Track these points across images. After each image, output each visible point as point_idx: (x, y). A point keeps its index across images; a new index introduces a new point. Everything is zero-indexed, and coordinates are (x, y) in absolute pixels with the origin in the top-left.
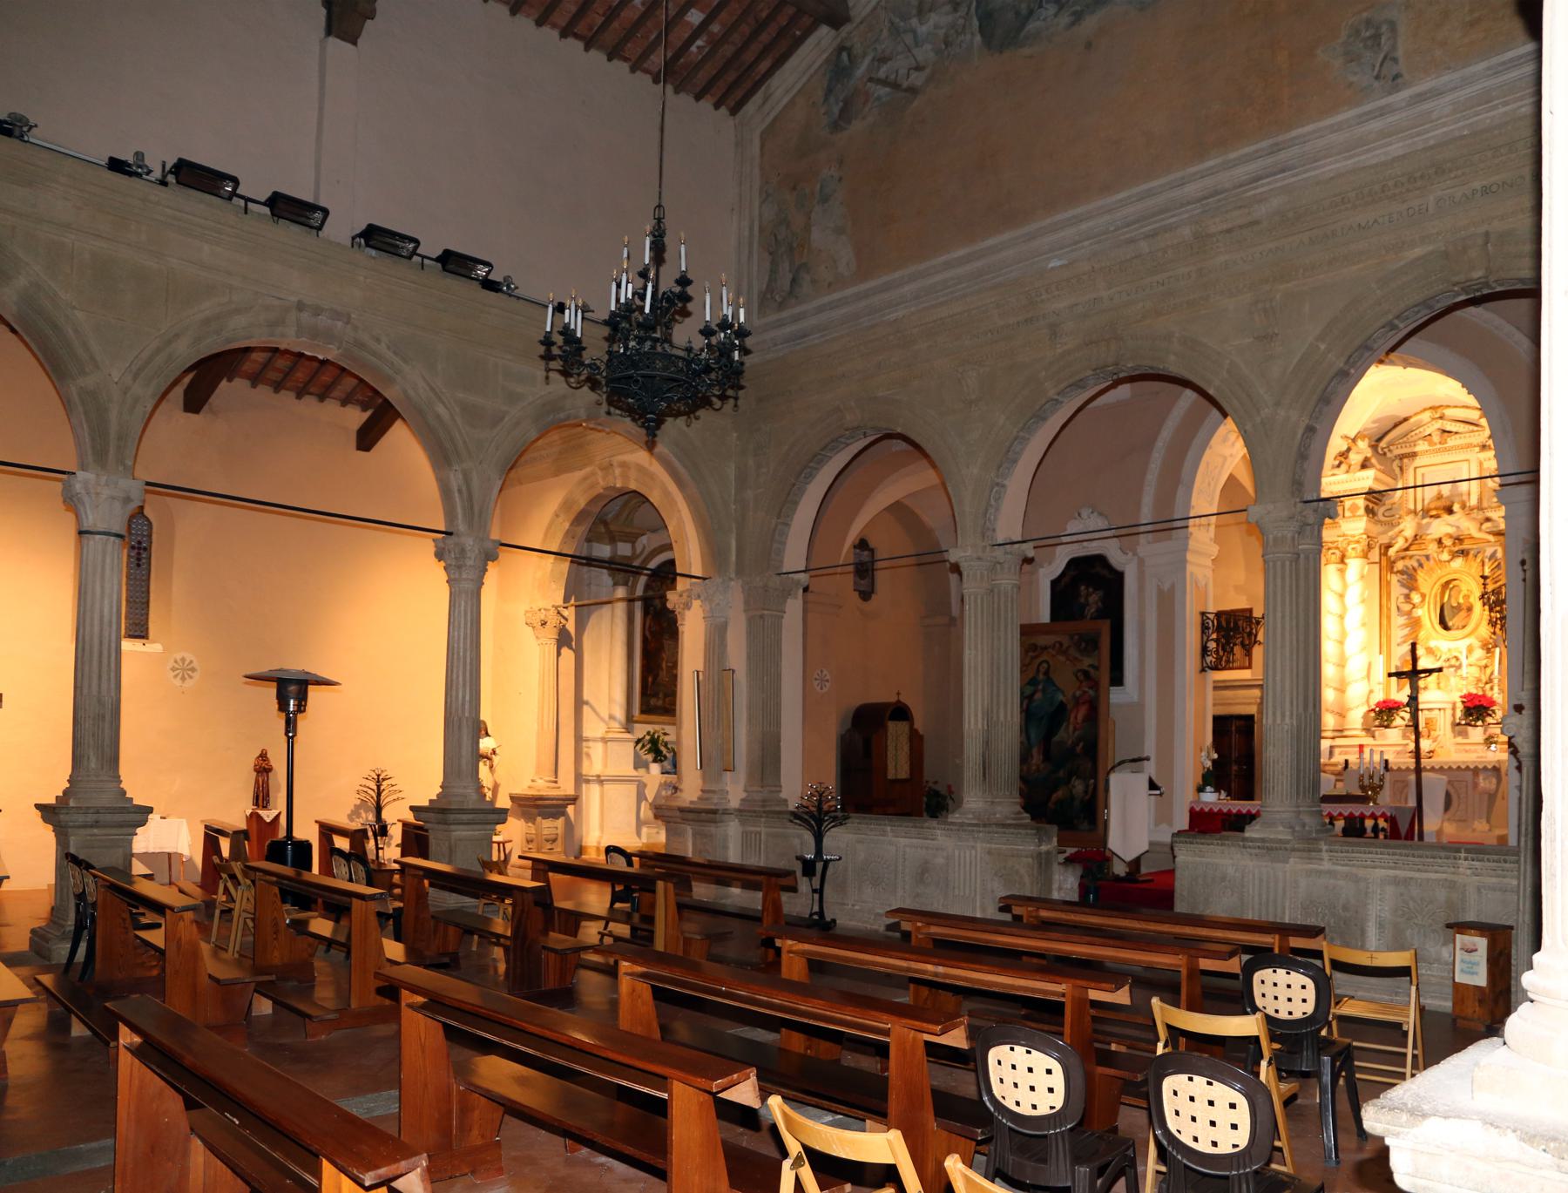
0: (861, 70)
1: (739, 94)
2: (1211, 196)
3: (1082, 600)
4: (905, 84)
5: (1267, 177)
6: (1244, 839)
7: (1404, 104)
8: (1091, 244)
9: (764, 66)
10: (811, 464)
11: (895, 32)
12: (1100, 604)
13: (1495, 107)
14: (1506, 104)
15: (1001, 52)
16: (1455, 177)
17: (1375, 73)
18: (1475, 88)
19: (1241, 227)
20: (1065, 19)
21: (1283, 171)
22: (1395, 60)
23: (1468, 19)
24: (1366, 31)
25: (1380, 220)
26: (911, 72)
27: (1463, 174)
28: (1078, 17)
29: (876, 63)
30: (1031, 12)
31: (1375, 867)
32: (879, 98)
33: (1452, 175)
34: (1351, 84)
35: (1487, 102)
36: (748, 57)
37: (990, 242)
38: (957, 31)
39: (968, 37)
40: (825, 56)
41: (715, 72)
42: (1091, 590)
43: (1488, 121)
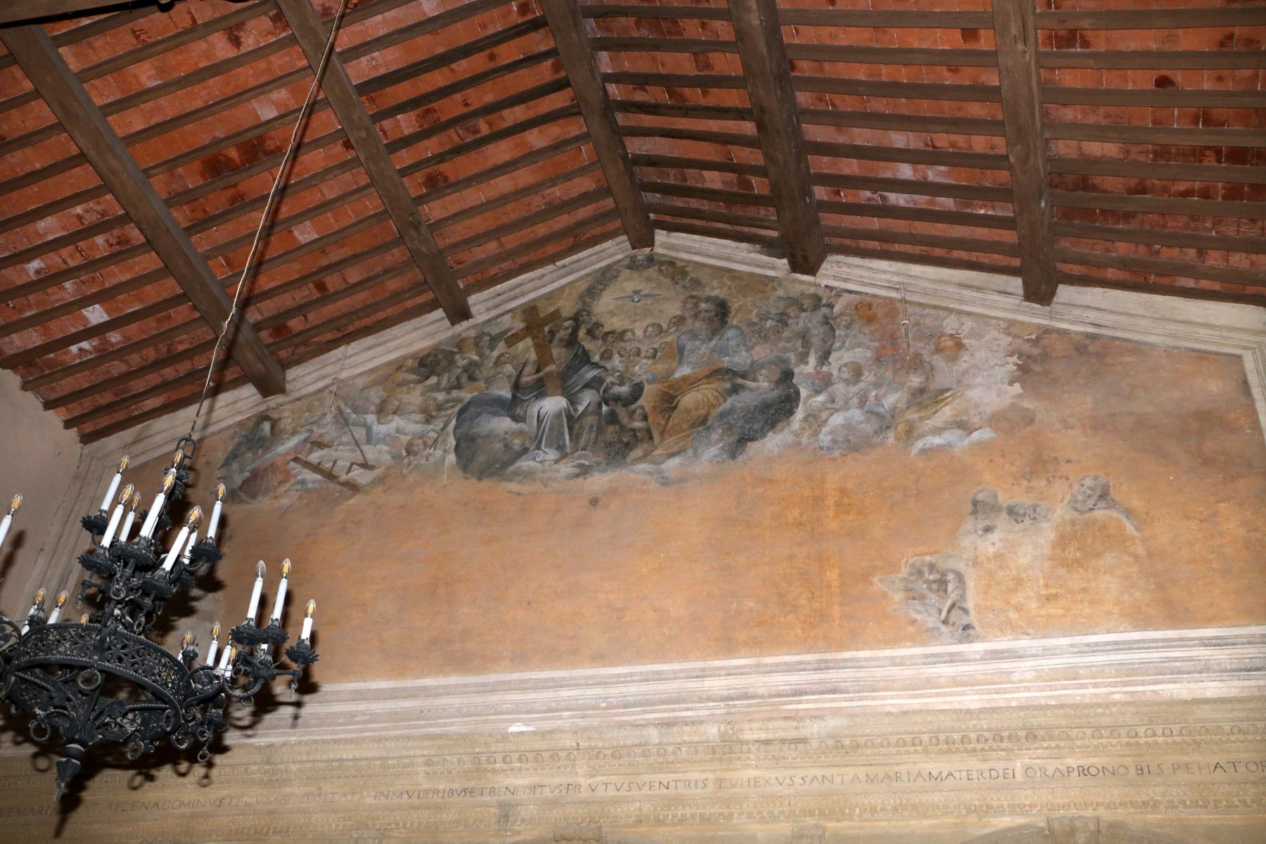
0: (288, 445)
1: (104, 421)
2: (739, 698)
4: (343, 477)
5: (813, 693)
7: (978, 657)
8: (571, 717)
9: (150, 404)
11: (340, 416)
14: (1096, 686)
15: (480, 479)
16: (1047, 748)
18: (1059, 661)
19: (783, 741)
20: (566, 468)
21: (834, 691)
22: (965, 611)
23: (1043, 592)
24: (930, 574)
25: (957, 775)
26: (354, 466)
27: (1058, 747)
28: (584, 471)
29: (308, 446)
30: (525, 451)
32: (303, 482)
33: (1045, 745)
34: (914, 622)
35: (1074, 679)
36: (138, 385)
37: (428, 682)
38: (425, 443)
39: (439, 453)
40: (239, 418)
41: (86, 385)
43: (1078, 698)
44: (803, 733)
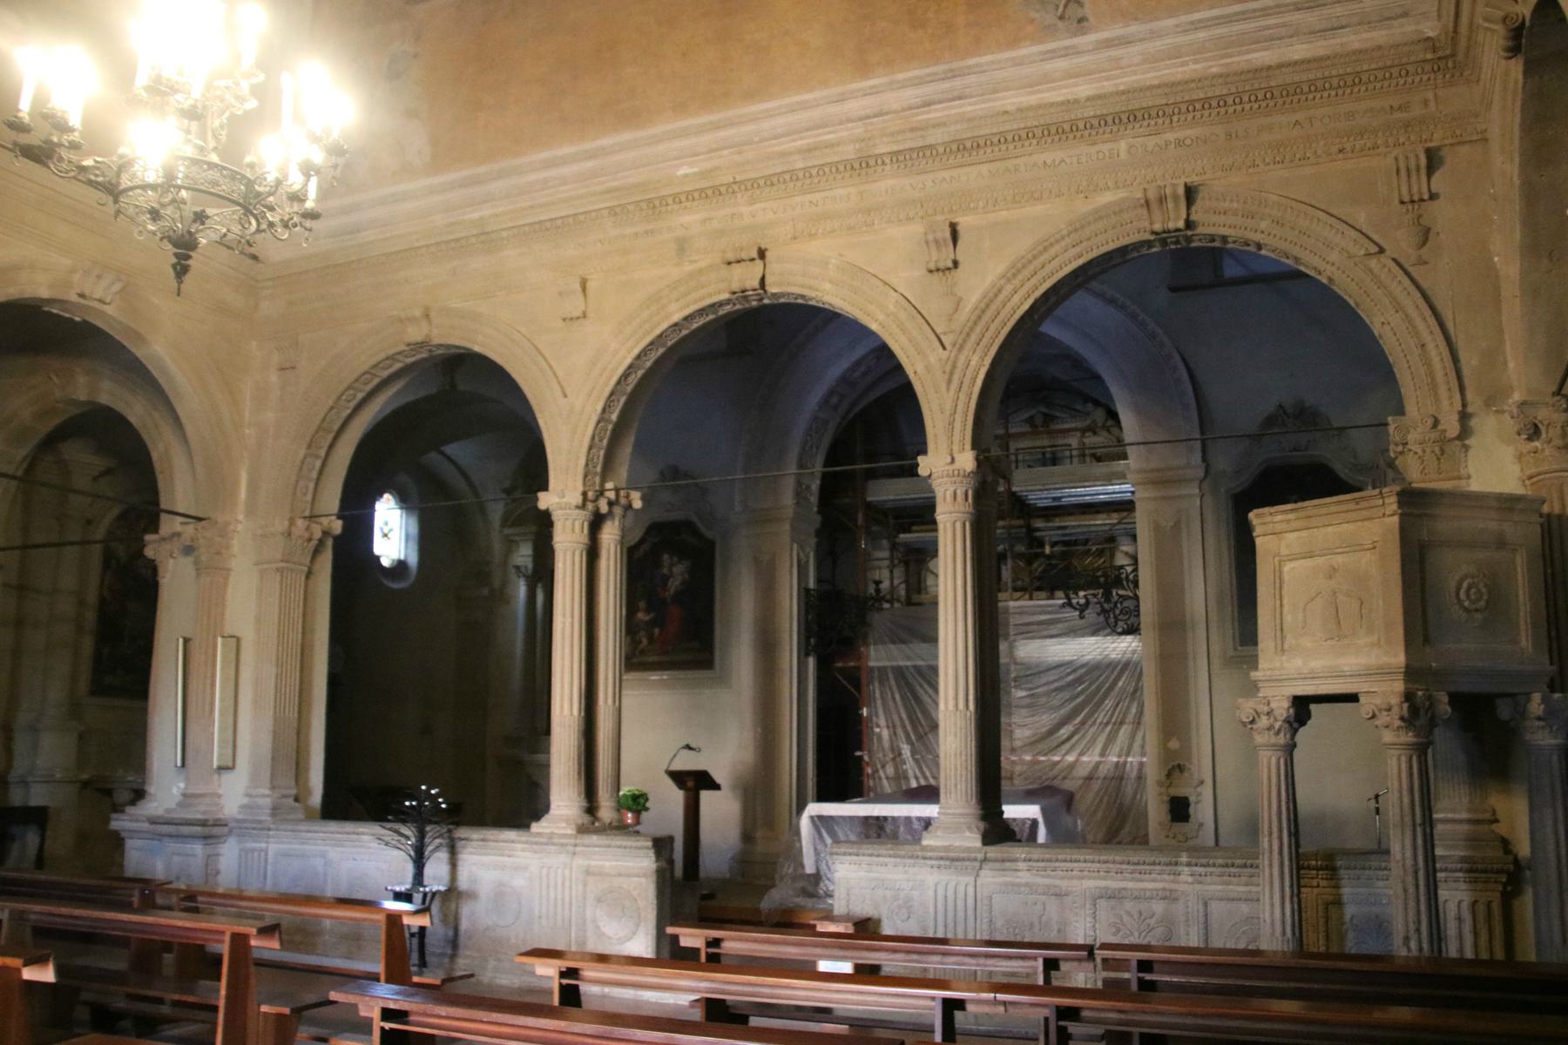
3: (665, 571)
6: (924, 849)
7: (1091, 47)
10: (356, 385)
12: (687, 576)
13: (1185, 64)
14: (1196, 62)
17: (1059, 13)
21: (960, 98)
25: (1068, 160)
31: (1083, 878)
34: (1032, 21)
37: (605, 141)
42: (675, 559)
44: (930, 141)
